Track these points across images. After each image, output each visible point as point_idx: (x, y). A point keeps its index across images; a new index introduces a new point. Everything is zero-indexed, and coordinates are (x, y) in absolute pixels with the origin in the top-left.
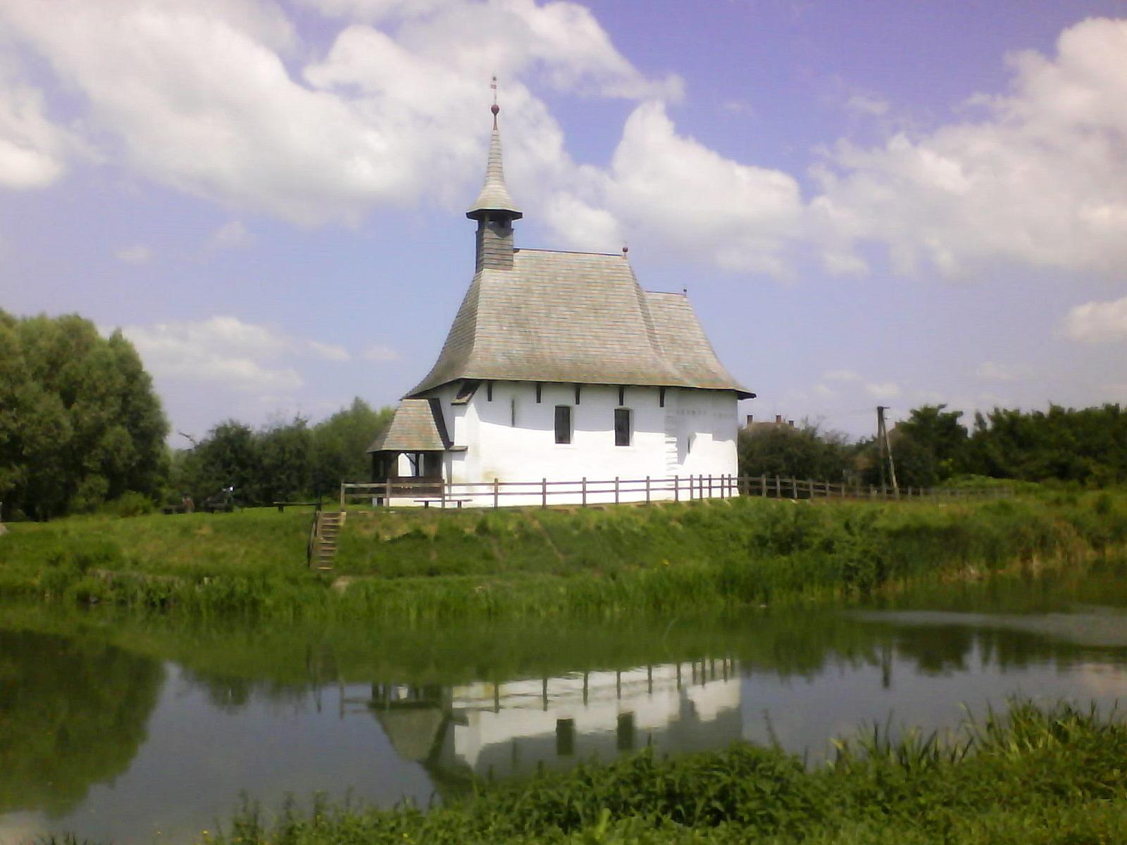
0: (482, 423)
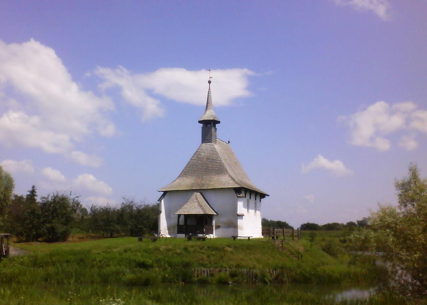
0: (243, 208)
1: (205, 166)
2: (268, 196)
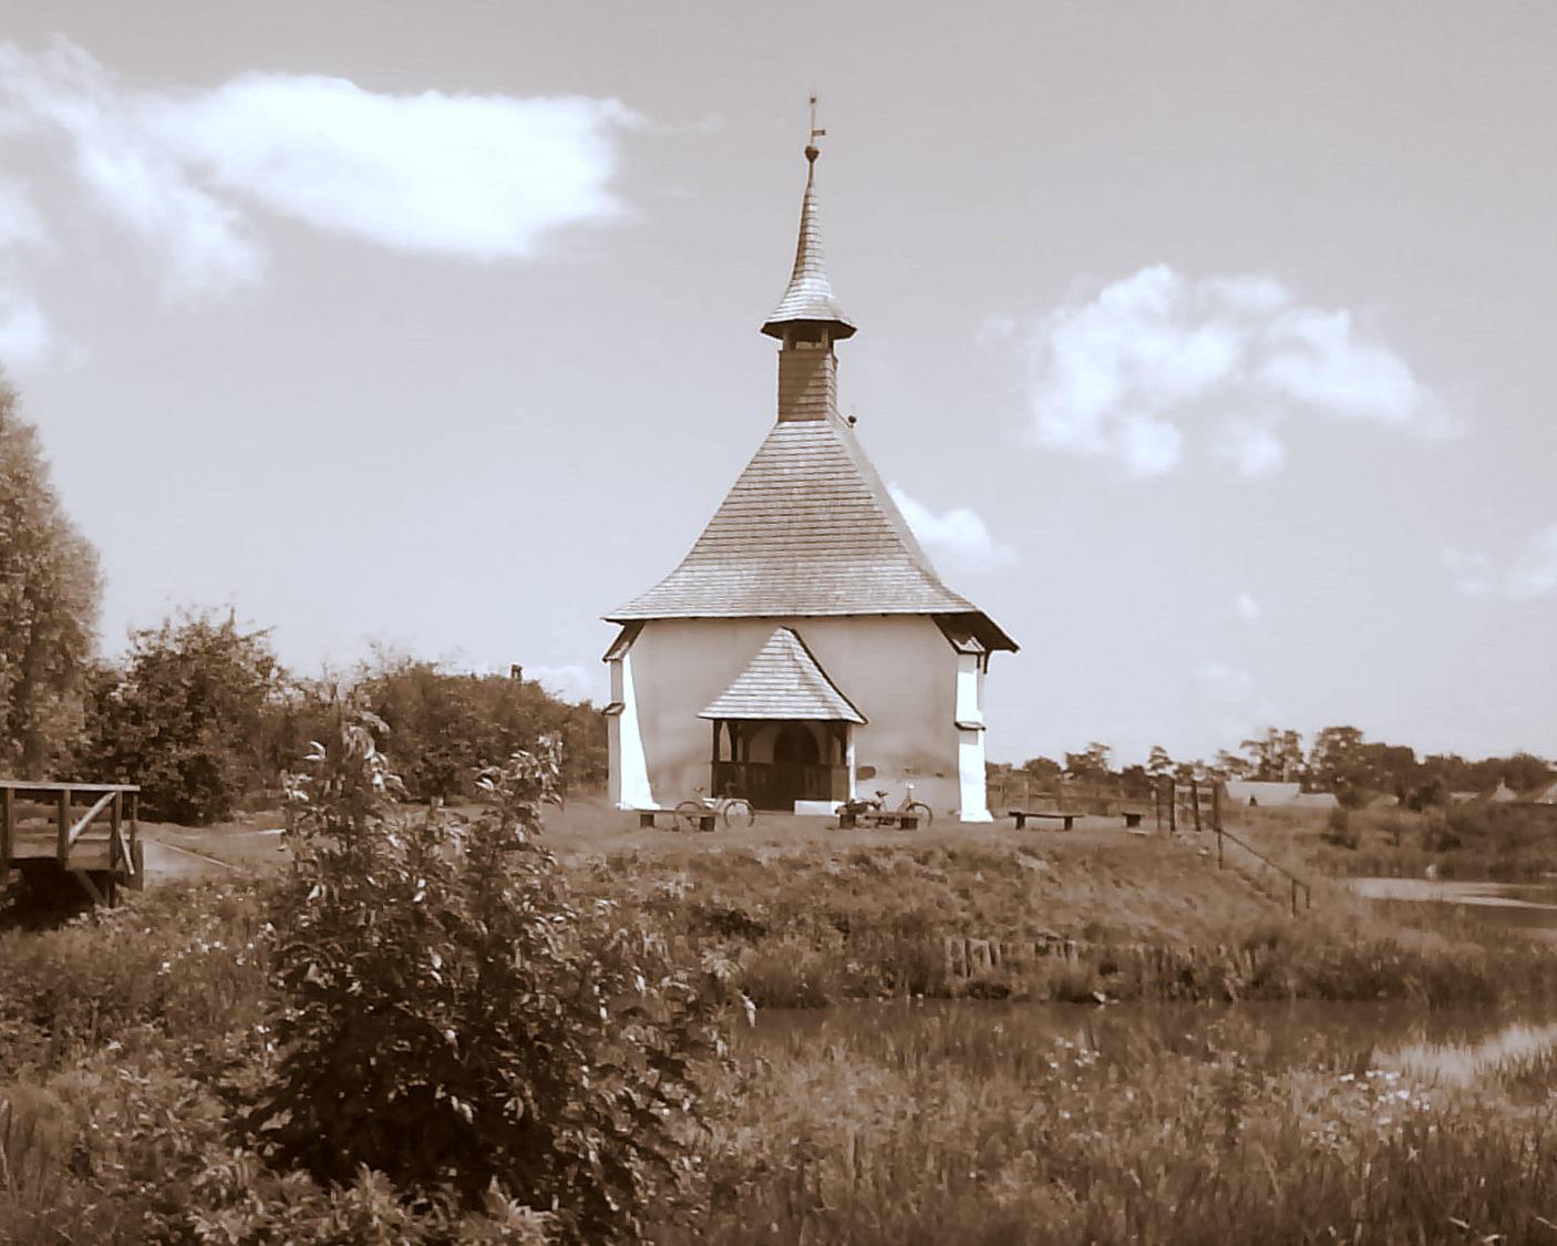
1: (800, 518)
2: (1014, 648)
